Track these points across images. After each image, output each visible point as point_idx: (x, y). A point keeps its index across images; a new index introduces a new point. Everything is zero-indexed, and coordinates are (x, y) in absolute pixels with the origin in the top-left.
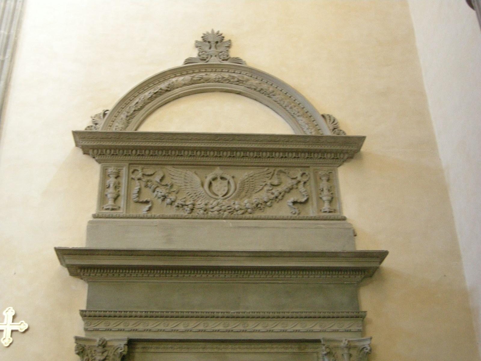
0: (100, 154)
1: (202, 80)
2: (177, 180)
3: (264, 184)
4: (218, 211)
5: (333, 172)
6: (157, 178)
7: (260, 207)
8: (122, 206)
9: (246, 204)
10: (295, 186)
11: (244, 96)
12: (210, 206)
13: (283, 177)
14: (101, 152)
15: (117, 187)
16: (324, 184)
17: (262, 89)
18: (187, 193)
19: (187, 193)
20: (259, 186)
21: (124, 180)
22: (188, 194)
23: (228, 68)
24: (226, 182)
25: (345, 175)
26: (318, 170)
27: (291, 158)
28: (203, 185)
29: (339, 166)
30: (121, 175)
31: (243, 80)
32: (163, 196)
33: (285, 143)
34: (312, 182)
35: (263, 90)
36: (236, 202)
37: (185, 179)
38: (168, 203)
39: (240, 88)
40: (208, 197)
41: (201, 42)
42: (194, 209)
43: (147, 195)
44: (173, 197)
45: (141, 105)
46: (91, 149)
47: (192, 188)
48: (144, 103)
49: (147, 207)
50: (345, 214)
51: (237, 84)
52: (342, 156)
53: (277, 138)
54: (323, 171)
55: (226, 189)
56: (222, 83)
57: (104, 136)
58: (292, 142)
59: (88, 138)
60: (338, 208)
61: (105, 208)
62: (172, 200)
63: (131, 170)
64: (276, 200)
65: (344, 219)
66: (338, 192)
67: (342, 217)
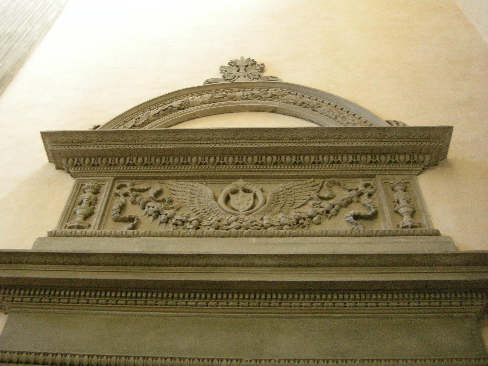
0: (76, 165)
1: (225, 98)
2: (180, 196)
3: (308, 198)
4: (237, 229)
5: (411, 182)
6: (151, 193)
7: (302, 224)
8: (93, 224)
9: (280, 219)
10: (355, 199)
11: (281, 114)
12: (224, 222)
13: (336, 190)
14: (77, 162)
15: (92, 203)
16: (400, 195)
17: (303, 103)
18: (193, 210)
19: (193, 210)
20: (301, 201)
21: (102, 197)
22: (194, 210)
23: (260, 86)
24: (251, 196)
25: (430, 187)
26: (387, 179)
27: (346, 163)
28: (216, 199)
29: (419, 174)
30: (100, 191)
31: (279, 95)
32: (155, 212)
33: (336, 140)
34: (381, 194)
35: (305, 104)
36: (265, 217)
37: (191, 193)
38: (161, 220)
39: (275, 104)
40: (222, 211)
41: (227, 67)
42: (200, 227)
43: (132, 211)
44: (170, 212)
45: (143, 121)
46: (64, 157)
47: (200, 203)
48: (148, 119)
49: (130, 225)
50: (437, 226)
51: (271, 101)
52: (421, 158)
53: (324, 133)
54: (397, 179)
55: (251, 203)
56: (251, 100)
57: (82, 138)
58: (345, 138)
59: (62, 142)
60: (424, 222)
61: (69, 225)
62: (169, 215)
63: (117, 185)
64: (327, 216)
65: (437, 233)
66: (422, 202)
67: (433, 230)
